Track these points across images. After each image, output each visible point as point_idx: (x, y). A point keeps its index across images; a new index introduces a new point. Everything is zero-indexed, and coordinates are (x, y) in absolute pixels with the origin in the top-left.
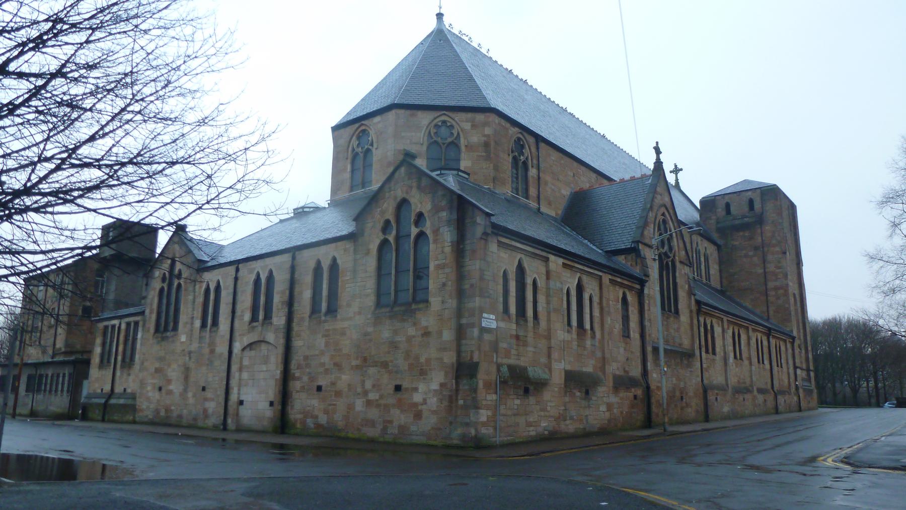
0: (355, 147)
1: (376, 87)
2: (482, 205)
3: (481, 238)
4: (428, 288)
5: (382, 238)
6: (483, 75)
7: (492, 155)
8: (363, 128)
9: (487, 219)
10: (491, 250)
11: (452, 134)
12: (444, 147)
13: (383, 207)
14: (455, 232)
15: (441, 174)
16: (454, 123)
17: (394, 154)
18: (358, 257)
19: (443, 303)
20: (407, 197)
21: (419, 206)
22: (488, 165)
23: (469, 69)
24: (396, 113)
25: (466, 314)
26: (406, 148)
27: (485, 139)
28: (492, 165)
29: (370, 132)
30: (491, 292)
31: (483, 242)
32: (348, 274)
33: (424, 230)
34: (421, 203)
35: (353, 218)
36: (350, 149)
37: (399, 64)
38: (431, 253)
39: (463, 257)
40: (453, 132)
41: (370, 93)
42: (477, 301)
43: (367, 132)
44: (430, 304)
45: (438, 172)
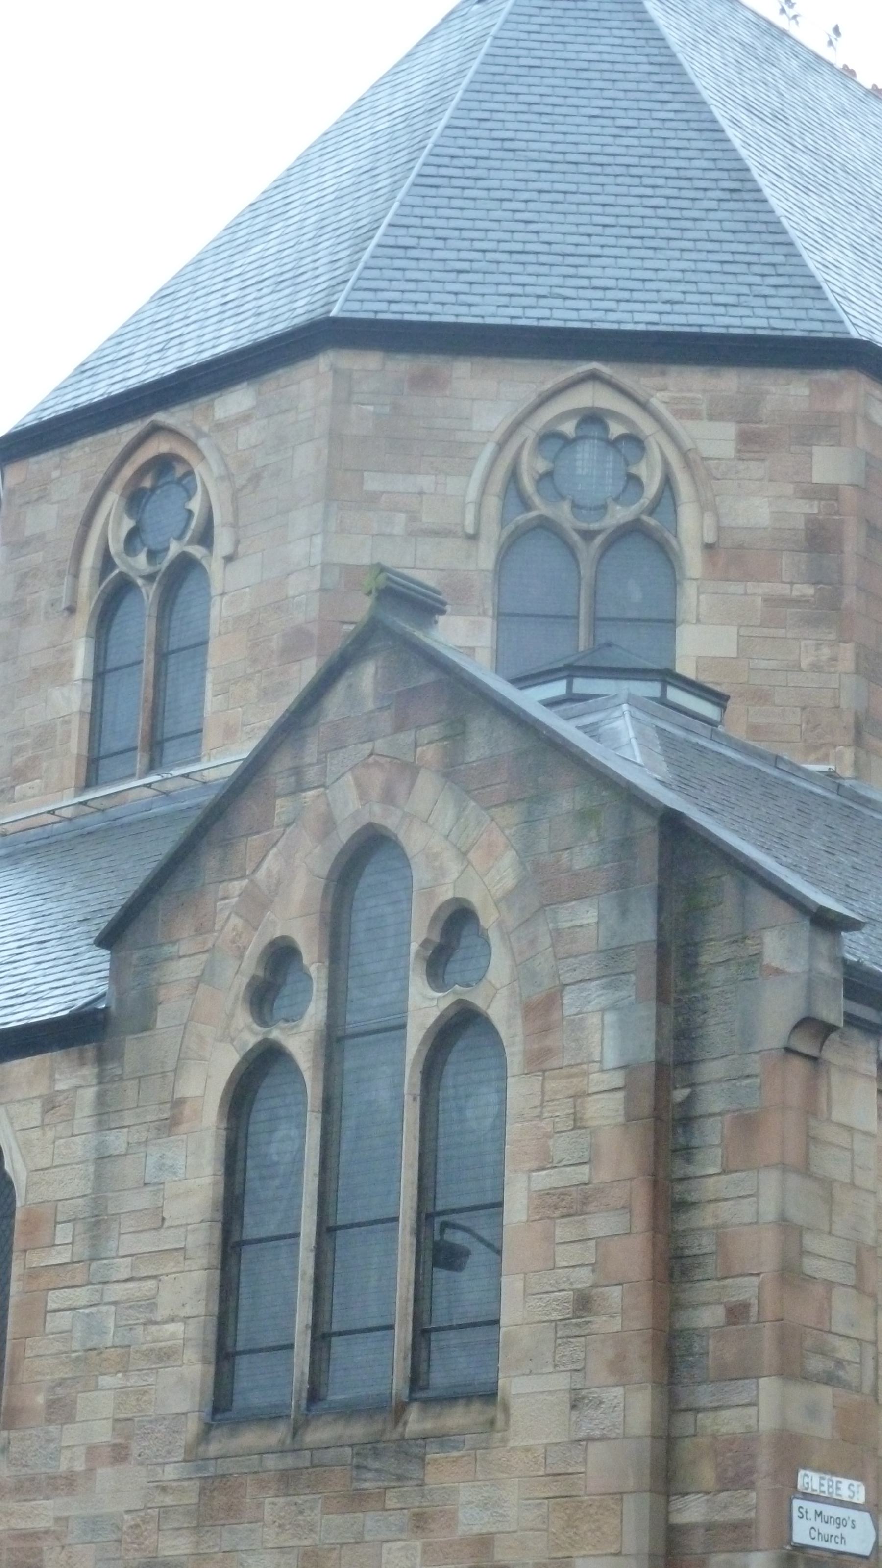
0: (116, 547)
1: (233, 227)
2: (794, 868)
3: (789, 1050)
4: (497, 1322)
5: (251, 1040)
6: (805, 162)
7: (851, 597)
8: (159, 446)
9: (823, 944)
10: (838, 1115)
11: (634, 480)
12: (588, 553)
13: (261, 874)
14: (647, 1011)
15: (571, 698)
16: (646, 426)
17: (323, 589)
18: (117, 1141)
19: (574, 1407)
20: (390, 821)
21: (454, 869)
22: (826, 652)
23: (730, 133)
24: (335, 371)
25: (707, 1474)
26: (388, 561)
27: (813, 507)
28: (847, 653)
29: (199, 470)
30: (845, 1350)
31: (798, 1066)
32: (64, 1233)
33: (478, 999)
34: (463, 854)
35: (101, 923)
36: (90, 559)
37: (357, 109)
38: (513, 1129)
39: (686, 1152)
40: (641, 470)
41: (197, 263)
42: (763, 1400)
43: (180, 471)
44: (506, 1409)
45: (558, 689)
